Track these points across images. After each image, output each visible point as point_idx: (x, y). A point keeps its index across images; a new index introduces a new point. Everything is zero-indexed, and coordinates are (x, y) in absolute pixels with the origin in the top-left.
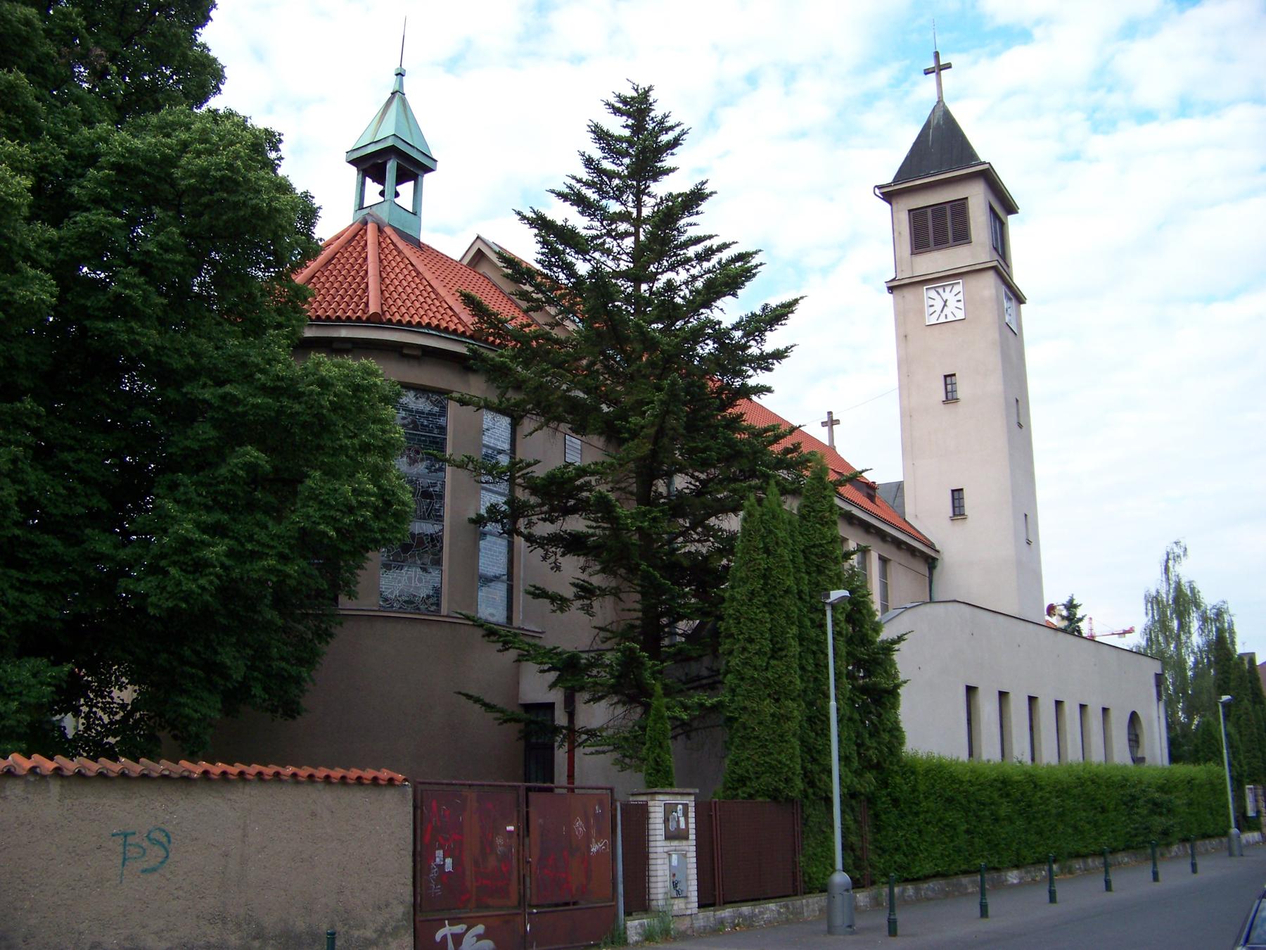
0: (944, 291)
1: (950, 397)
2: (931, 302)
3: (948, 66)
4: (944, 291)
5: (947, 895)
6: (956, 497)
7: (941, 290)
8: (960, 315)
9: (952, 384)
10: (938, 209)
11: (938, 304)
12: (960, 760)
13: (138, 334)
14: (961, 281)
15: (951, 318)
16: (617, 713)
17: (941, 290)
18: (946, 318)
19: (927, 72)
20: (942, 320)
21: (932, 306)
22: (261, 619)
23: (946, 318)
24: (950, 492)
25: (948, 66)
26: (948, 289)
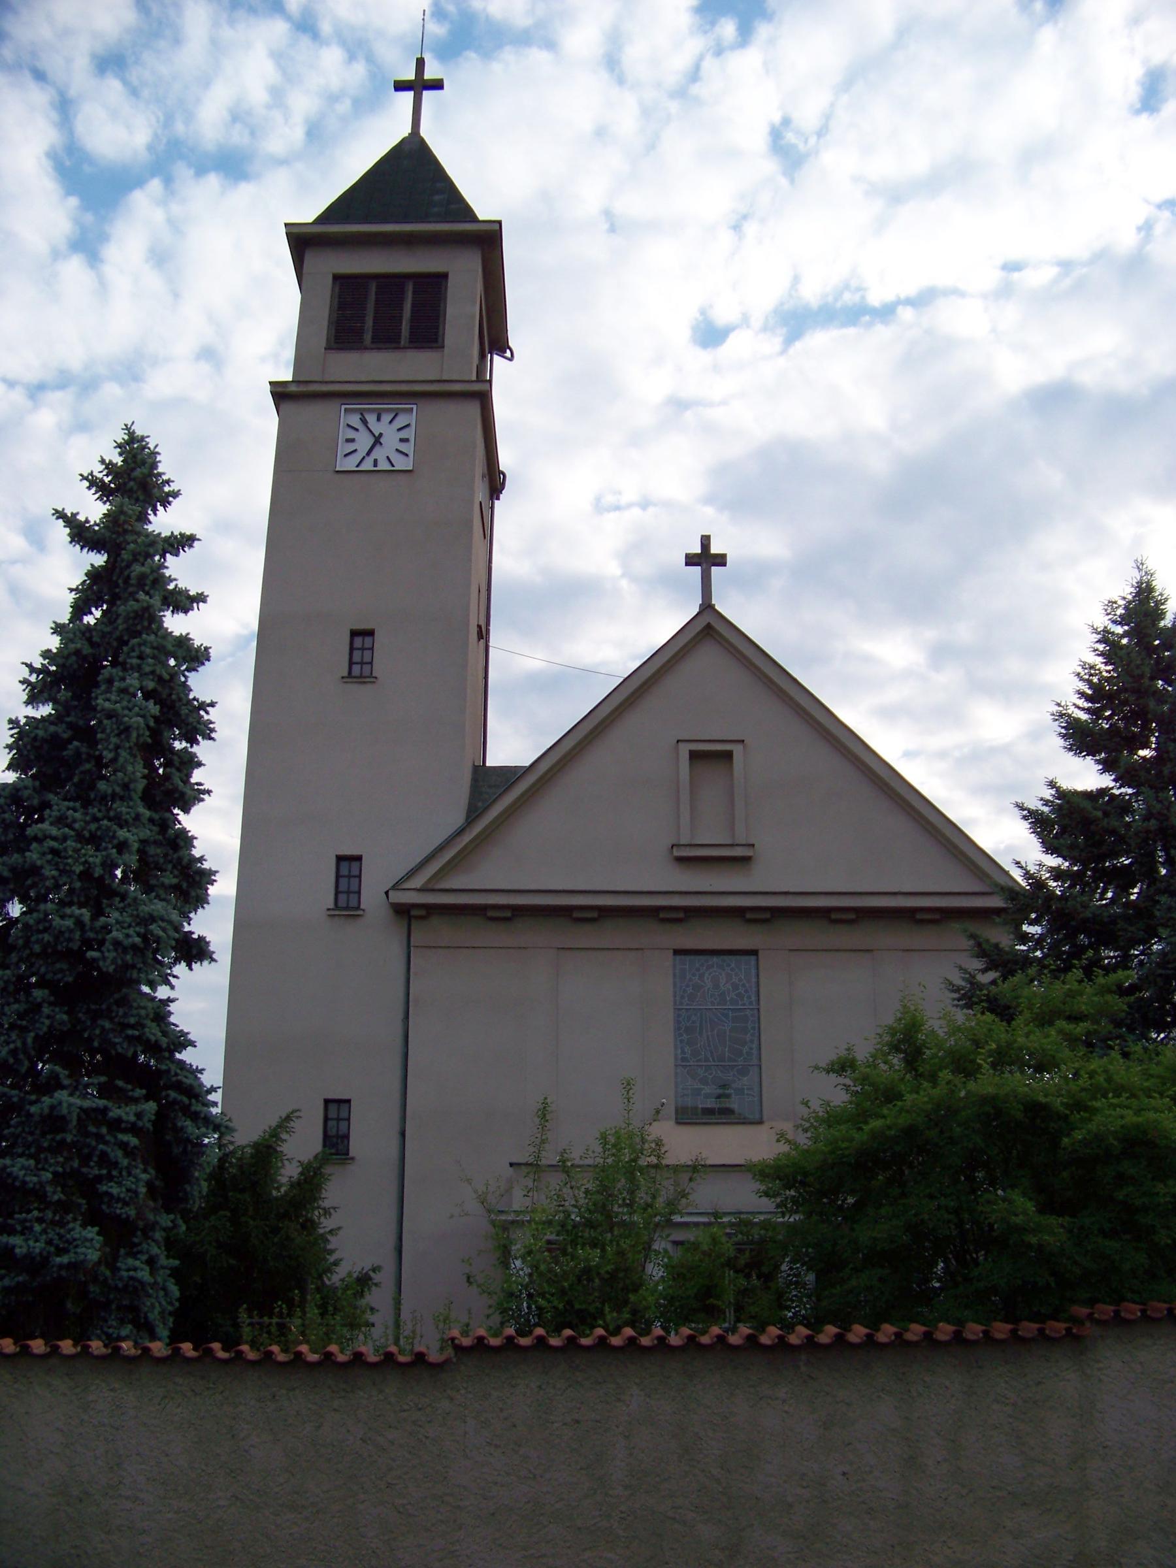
0: (379, 419)
1: (342, 903)
2: (351, 434)
3: (437, 85)
4: (379, 419)
5: (782, 304)
6: (333, 1113)
7: (371, 419)
8: (401, 464)
9: (348, 892)
10: (391, 284)
11: (364, 441)
12: (199, 963)
13: (779, 1212)
14: (415, 407)
15: (383, 465)
16: (892, 1057)
17: (371, 419)
18: (375, 465)
19: (400, 86)
20: (368, 465)
21: (352, 440)
22: (322, 1245)
23: (375, 465)
24: (333, 861)
25: (437, 85)
26: (386, 418)
